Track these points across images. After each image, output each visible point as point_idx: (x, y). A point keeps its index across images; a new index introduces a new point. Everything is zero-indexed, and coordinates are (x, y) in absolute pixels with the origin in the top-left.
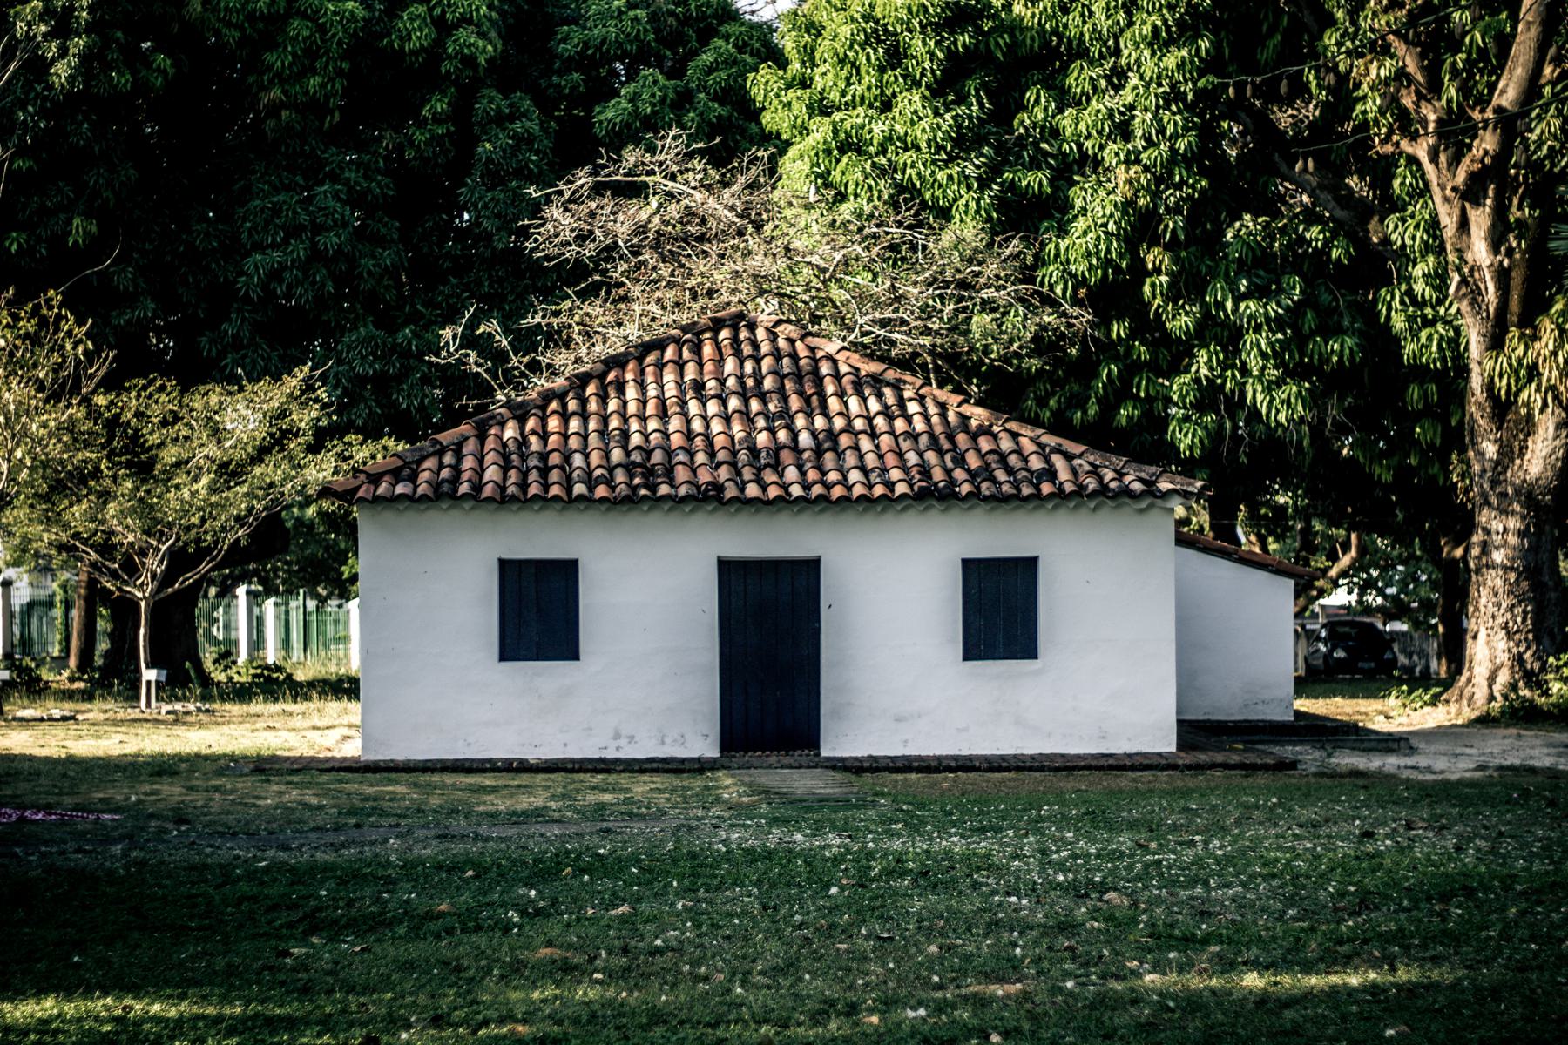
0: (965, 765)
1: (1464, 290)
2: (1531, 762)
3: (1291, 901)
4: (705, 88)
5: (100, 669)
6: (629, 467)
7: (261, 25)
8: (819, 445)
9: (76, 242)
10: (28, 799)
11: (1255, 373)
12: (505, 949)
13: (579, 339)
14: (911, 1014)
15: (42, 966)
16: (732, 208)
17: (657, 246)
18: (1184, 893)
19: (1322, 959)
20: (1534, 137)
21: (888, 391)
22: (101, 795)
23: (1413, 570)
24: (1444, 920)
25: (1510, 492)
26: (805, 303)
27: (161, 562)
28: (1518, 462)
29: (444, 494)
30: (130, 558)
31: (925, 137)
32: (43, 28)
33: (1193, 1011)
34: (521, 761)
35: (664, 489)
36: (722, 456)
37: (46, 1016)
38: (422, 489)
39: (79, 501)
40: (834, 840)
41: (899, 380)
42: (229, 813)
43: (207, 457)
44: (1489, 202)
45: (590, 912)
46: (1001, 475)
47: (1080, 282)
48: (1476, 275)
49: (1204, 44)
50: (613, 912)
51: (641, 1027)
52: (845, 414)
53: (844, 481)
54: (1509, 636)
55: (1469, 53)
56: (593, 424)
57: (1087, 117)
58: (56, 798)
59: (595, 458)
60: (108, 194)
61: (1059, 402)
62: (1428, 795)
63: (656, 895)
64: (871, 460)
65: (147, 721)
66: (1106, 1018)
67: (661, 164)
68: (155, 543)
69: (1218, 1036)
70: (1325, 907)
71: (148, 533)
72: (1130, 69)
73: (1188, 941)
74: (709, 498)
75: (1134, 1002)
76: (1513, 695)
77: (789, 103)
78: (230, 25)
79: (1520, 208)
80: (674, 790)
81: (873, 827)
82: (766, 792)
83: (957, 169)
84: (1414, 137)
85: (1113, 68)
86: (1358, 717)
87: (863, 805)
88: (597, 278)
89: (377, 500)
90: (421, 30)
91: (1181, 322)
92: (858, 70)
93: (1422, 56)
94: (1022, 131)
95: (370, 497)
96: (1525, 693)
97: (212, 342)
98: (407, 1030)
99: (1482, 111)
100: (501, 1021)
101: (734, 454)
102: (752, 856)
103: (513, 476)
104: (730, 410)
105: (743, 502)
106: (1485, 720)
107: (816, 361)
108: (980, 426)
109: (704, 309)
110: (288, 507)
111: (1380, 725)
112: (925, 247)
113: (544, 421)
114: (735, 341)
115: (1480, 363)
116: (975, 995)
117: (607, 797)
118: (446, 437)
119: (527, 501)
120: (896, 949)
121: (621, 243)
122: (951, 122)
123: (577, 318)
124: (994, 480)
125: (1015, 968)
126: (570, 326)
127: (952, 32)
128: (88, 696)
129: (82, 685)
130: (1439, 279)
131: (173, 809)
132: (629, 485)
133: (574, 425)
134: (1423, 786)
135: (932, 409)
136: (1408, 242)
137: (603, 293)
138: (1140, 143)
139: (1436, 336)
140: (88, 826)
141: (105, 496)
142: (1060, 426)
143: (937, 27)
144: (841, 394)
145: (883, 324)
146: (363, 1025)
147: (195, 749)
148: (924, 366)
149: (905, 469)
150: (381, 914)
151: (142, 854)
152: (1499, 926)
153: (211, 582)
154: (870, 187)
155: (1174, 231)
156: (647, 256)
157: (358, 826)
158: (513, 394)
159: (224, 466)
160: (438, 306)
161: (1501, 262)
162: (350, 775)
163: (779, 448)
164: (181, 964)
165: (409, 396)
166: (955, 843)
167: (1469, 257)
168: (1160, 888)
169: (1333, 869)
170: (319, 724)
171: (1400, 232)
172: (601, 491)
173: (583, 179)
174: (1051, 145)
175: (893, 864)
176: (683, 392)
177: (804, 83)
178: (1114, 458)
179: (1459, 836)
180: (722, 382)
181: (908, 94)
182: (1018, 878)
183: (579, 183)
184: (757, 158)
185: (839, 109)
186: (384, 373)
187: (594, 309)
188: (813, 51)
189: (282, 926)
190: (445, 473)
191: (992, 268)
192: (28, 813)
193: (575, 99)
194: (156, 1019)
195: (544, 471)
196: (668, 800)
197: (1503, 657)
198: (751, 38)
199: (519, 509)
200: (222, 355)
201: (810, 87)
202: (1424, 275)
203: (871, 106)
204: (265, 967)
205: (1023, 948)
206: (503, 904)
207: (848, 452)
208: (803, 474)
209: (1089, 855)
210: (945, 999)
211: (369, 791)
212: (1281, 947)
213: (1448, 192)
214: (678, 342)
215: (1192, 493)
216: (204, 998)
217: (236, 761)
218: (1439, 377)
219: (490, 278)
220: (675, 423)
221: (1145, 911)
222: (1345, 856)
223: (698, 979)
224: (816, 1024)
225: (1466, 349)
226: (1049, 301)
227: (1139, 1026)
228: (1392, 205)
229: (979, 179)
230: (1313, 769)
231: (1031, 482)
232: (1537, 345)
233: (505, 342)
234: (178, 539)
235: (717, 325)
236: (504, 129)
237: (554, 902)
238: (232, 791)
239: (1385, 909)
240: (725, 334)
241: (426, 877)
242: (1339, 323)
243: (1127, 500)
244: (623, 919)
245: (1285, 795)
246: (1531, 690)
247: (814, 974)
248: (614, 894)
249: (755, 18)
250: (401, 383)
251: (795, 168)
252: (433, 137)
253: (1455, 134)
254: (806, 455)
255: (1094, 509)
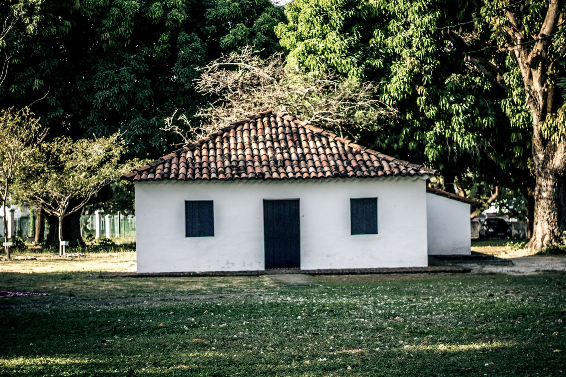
0: (352, 272)
1: (531, 100)
2: (555, 269)
3: (461, 319)
4: (260, 30)
5: (45, 241)
6: (231, 167)
7: (100, 10)
8: (299, 158)
9: (36, 88)
10: (17, 289)
11: (457, 130)
12: (181, 339)
13: (214, 121)
14: (321, 360)
15: (19, 347)
16: (269, 74)
17: (242, 87)
18: (423, 317)
19: (467, 339)
20: (555, 44)
21: (323, 139)
22: (44, 287)
23: (518, 199)
24: (513, 325)
25: (548, 172)
26: (295, 107)
27: (66, 203)
28: (551, 161)
29: (165, 178)
30: (55, 201)
31: (338, 48)
32: (24, 13)
33: (419, 358)
34: (194, 273)
35: (243, 175)
36: (264, 163)
37: (19, 364)
38: (158, 176)
39: (37, 182)
40: (301, 299)
41: (327, 135)
42: (88, 292)
43: (82, 165)
44: (539, 68)
45: (213, 326)
46: (364, 169)
47: (394, 98)
48: (535, 94)
49: (438, 13)
50: (221, 326)
51: (226, 365)
52: (308, 147)
53: (308, 172)
54: (549, 223)
55: (532, 15)
56: (218, 152)
57: (396, 40)
58: (28, 288)
59: (219, 164)
60: (48, 70)
61: (389, 141)
62: (515, 281)
63: (236, 320)
64: (317, 164)
65: (62, 260)
66: (388, 361)
67: (243, 58)
68: (64, 196)
69: (426, 366)
70: (472, 321)
71: (62, 193)
72: (411, 22)
73: (422, 334)
74: (260, 178)
75: (399, 355)
76: (550, 245)
77: (289, 37)
78: (89, 10)
79: (552, 70)
80: (247, 282)
81: (316, 295)
82: (280, 283)
83: (350, 59)
84: (513, 45)
85: (405, 22)
86: (496, 253)
87: (314, 287)
88: (221, 99)
89: (141, 180)
90: (159, 11)
91: (431, 113)
92: (313, 24)
93: (515, 16)
94: (372, 45)
95: (139, 179)
96: (554, 243)
97: (84, 123)
98: (145, 368)
99: (537, 36)
100: (178, 364)
101: (269, 162)
102: (271, 305)
103: (190, 171)
104: (267, 147)
105: (272, 179)
106: (540, 254)
107: (298, 128)
108: (356, 151)
109: (259, 110)
110: (113, 182)
111: (503, 256)
112: (337, 87)
113: (201, 151)
114: (269, 122)
115: (537, 126)
116: (344, 353)
117: (223, 285)
118: (166, 157)
119: (195, 180)
120: (319, 338)
121: (229, 87)
122: (347, 42)
123: (214, 114)
124: (361, 170)
125: (359, 344)
126: (211, 117)
127: (347, 10)
128: (41, 251)
129: (39, 247)
130: (522, 95)
131: (69, 291)
132: (231, 174)
133: (212, 152)
134: (514, 277)
135: (339, 145)
136: (511, 83)
137: (223, 105)
138: (415, 49)
139: (522, 117)
140: (38, 298)
141: (46, 180)
142: (389, 151)
143: (342, 9)
144: (307, 140)
145: (323, 114)
146: (129, 366)
147: (78, 270)
148: (338, 129)
149: (330, 167)
150: (140, 327)
151: (56, 307)
152: (532, 327)
153: (86, 209)
154: (319, 67)
155: (427, 81)
156: (239, 91)
157: (133, 296)
158: (191, 141)
159: (89, 168)
160: (165, 110)
161: (544, 90)
162: (133, 278)
163: (284, 160)
164: (68, 345)
165: (155, 142)
166: (345, 300)
167: (532, 88)
168: (414, 315)
169: (477, 308)
170: (123, 260)
171: (509, 79)
172: (221, 176)
173: (215, 64)
174: (383, 50)
175: (321, 308)
176: (251, 140)
177: (295, 29)
178: (404, 162)
179: (524, 296)
180: (264, 136)
181: (331, 33)
182: (365, 312)
183: (214, 65)
184: (277, 56)
185: (307, 38)
186: (146, 134)
187: (220, 110)
188: (297, 18)
189: (104, 332)
190: (166, 170)
191: (362, 94)
192: (17, 293)
193: (213, 35)
194: (57, 365)
195: (201, 169)
196: (245, 286)
197: (547, 231)
198: (276, 12)
199: (192, 183)
200: (87, 128)
201: (296, 30)
202: (517, 95)
203: (319, 37)
204: (97, 346)
205: (363, 337)
206: (182, 324)
207: (309, 161)
208: (293, 169)
209: (391, 304)
210: (333, 355)
211: (139, 284)
212: (454, 335)
213: (525, 65)
214: (249, 122)
215: (432, 174)
216: (75, 357)
217: (92, 274)
218: (523, 131)
219: (183, 99)
220: (248, 152)
221: (408, 323)
222: (482, 303)
223: (248, 349)
224: (288, 364)
225: (532, 121)
226: (383, 106)
227: (400, 363)
228: (505, 69)
229: (357, 63)
230: (477, 272)
231: (374, 171)
232: (557, 119)
233: (188, 123)
234: (72, 195)
235: (262, 116)
236: (188, 46)
237: (200, 322)
238: (90, 285)
239: (493, 322)
240: (265, 119)
241: (156, 314)
242: (487, 113)
243: (409, 177)
244: (224, 328)
245: (465, 282)
246: (557, 243)
247: (289, 346)
248: (222, 320)
249: (278, 5)
250: (152, 137)
251: (292, 60)
252: (162, 49)
253: (527, 44)
254: (294, 162)
255: (398, 180)
